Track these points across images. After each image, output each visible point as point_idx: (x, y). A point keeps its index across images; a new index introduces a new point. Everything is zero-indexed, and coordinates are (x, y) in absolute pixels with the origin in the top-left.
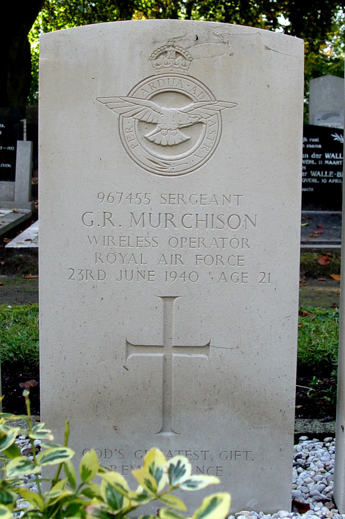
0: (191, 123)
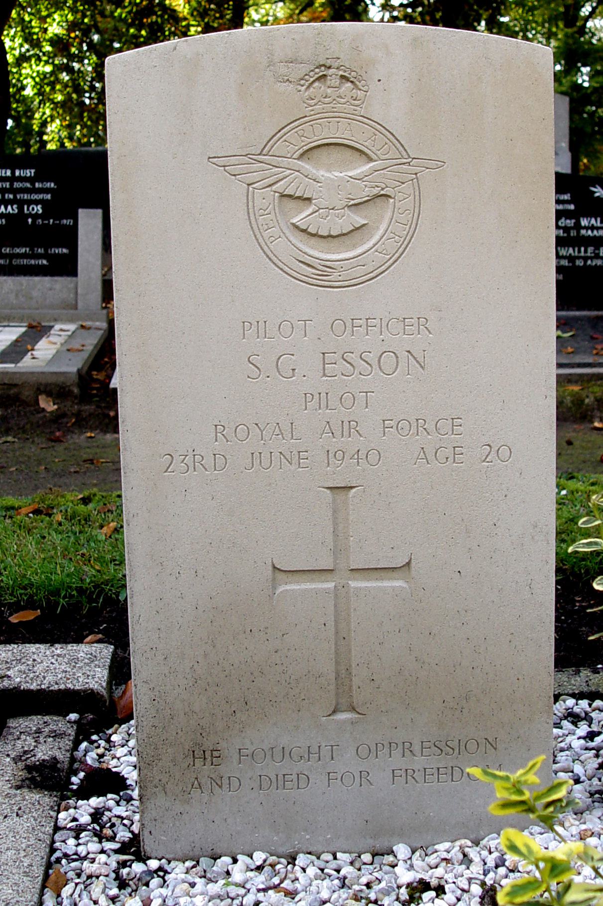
0: (368, 196)
